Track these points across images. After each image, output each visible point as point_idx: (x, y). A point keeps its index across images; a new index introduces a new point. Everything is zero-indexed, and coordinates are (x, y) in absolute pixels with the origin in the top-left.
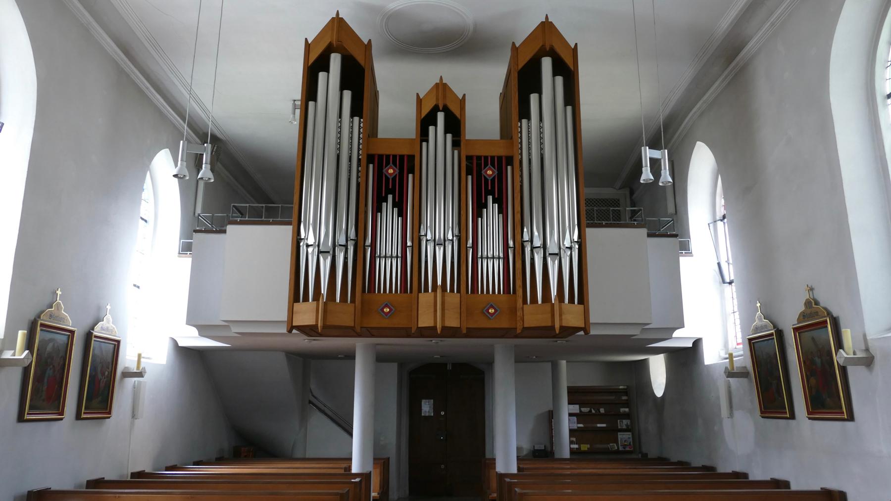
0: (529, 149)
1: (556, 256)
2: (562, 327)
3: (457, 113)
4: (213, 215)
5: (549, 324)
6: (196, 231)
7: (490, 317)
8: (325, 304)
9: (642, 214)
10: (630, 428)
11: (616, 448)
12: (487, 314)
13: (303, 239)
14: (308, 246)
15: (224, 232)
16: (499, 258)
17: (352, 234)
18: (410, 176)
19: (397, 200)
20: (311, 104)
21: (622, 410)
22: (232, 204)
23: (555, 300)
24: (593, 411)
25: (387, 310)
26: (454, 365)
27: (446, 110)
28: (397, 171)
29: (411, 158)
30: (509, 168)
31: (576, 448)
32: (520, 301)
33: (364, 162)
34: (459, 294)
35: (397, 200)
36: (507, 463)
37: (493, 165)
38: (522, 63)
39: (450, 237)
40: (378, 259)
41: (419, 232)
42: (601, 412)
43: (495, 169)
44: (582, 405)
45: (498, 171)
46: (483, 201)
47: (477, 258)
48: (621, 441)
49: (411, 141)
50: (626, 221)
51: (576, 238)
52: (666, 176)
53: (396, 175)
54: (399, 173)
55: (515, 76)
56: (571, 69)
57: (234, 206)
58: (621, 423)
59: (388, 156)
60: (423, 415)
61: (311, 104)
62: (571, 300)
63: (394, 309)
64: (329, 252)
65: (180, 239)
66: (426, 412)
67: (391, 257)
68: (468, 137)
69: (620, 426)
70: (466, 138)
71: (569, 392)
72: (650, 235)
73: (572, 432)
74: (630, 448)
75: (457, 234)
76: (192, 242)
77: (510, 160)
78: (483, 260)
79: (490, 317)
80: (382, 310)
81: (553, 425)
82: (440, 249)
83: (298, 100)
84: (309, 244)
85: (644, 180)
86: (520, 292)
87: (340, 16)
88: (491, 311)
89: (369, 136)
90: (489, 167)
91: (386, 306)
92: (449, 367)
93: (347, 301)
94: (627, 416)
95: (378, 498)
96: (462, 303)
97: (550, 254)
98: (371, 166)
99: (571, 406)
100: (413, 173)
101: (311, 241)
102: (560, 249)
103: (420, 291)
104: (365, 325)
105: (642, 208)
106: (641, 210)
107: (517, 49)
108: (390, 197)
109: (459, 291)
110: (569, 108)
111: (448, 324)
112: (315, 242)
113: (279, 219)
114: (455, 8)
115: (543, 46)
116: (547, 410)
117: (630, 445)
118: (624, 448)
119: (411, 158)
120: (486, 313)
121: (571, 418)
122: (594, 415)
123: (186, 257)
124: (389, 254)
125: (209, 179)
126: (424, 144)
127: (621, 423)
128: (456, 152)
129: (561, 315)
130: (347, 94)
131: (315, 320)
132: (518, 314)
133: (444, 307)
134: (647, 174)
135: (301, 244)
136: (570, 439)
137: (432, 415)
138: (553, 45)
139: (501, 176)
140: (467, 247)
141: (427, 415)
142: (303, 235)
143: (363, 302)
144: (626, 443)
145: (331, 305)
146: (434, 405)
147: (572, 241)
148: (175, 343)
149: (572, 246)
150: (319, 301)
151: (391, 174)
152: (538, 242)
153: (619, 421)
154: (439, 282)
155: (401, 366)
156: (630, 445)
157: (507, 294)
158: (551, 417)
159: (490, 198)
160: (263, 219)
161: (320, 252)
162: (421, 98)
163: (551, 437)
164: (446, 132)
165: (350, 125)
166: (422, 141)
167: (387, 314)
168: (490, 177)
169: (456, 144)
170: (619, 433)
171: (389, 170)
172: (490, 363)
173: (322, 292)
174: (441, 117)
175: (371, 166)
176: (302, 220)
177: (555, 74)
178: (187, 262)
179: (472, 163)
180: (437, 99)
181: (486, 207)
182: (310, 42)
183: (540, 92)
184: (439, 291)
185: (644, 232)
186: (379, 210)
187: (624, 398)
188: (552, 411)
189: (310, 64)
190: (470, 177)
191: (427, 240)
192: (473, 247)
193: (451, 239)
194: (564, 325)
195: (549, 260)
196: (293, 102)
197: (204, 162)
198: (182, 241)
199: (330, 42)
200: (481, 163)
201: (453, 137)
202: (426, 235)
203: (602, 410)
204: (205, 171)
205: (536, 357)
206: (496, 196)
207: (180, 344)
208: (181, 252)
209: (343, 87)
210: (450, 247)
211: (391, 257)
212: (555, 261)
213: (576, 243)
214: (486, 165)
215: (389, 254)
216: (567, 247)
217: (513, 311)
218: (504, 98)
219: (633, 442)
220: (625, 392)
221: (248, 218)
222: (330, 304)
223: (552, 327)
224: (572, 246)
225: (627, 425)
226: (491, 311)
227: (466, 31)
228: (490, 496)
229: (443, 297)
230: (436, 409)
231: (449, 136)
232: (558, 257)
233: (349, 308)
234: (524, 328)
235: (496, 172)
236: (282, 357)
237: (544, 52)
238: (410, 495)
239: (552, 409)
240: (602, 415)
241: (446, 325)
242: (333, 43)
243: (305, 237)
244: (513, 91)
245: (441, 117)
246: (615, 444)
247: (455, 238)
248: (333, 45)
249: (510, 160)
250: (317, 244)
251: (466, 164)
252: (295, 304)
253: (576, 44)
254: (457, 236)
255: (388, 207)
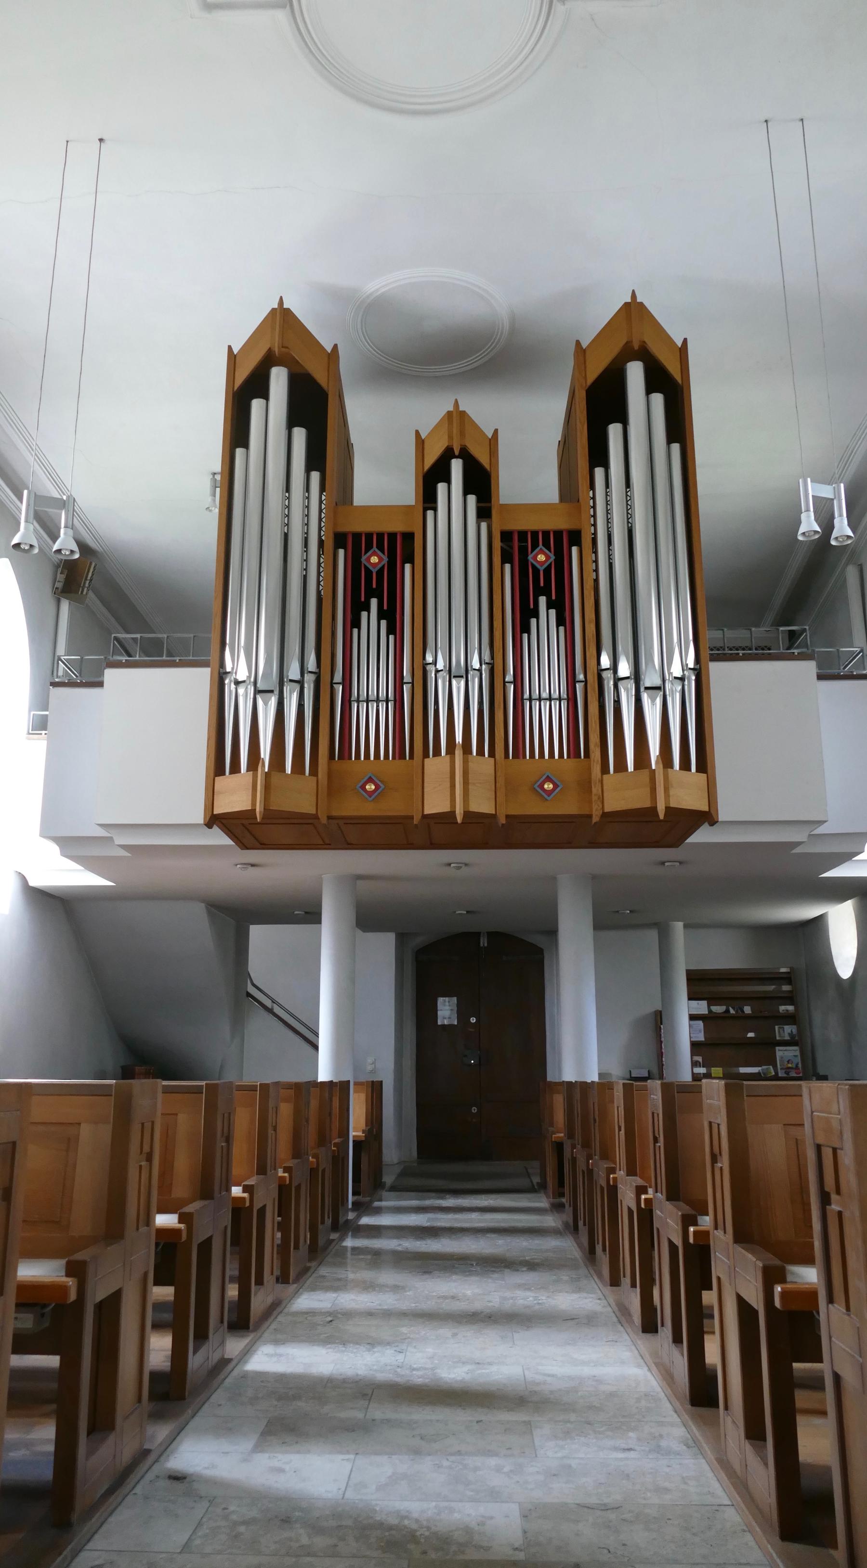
0: (608, 521)
1: (657, 691)
2: (668, 809)
3: (484, 460)
4: (82, 658)
5: (647, 804)
6: (54, 684)
7: (546, 796)
8: (267, 775)
9: (806, 638)
10: (797, 1038)
11: (774, 1074)
12: (541, 792)
13: (229, 673)
14: (237, 683)
15: (100, 684)
16: (560, 699)
17: (311, 664)
18: (408, 567)
19: (385, 607)
20: (239, 452)
21: (782, 1008)
22: (113, 635)
23: (657, 762)
24: (732, 1011)
25: (370, 787)
26: (491, 935)
27: (466, 455)
28: (385, 559)
29: (409, 537)
30: (575, 550)
31: (703, 1074)
32: (596, 769)
33: (329, 545)
34: (493, 759)
35: (385, 607)
36: (581, 1062)
37: (547, 545)
38: (593, 374)
39: (476, 664)
40: (356, 705)
41: (424, 658)
42: (746, 1012)
43: (550, 551)
44: (712, 1000)
45: (555, 555)
46: (532, 606)
47: (523, 699)
48: (781, 1061)
49: (407, 510)
50: (780, 650)
51: (691, 664)
52: (841, 528)
53: (383, 566)
54: (388, 562)
55: (581, 395)
56: (678, 383)
57: (116, 639)
58: (781, 1031)
59: (369, 536)
60: (439, 1023)
61: (239, 452)
62: (685, 764)
63: (382, 786)
64: (272, 691)
65: (30, 711)
66: (444, 1018)
67: (378, 700)
68: (502, 501)
69: (780, 1036)
70: (501, 502)
71: (688, 980)
72: (820, 677)
73: (695, 1046)
74: (798, 1074)
75: (487, 661)
76: (47, 716)
77: (575, 537)
78: (533, 702)
79: (546, 796)
80: (363, 787)
81: (662, 1035)
82: (459, 683)
83: (218, 473)
84: (240, 680)
85: (804, 534)
86: (596, 753)
87: (285, 306)
88: (548, 786)
89: (336, 504)
90: (541, 549)
91: (370, 780)
92: (484, 942)
93: (303, 773)
94: (790, 1019)
95: (363, 1139)
96: (498, 774)
97: (647, 688)
98: (341, 552)
99: (694, 1003)
100: (411, 561)
101: (242, 674)
102: (664, 681)
103: (426, 755)
104: (335, 813)
105: (807, 628)
106: (805, 630)
107: (584, 351)
108: (374, 602)
109: (492, 754)
110: (676, 447)
111: (474, 807)
112: (249, 677)
113: (191, 658)
114: (480, 288)
115: (627, 343)
116: (654, 1010)
117: (797, 1067)
118: (787, 1073)
119: (409, 537)
120: (539, 790)
121: (693, 1022)
122: (733, 1017)
123: (38, 739)
124: (373, 694)
125: (72, 552)
126: (430, 513)
127: (781, 1031)
128: (484, 526)
129: (667, 789)
130: (300, 435)
131: (250, 802)
132: (594, 790)
133: (468, 779)
134: (809, 523)
135: (227, 682)
136: (692, 1058)
137: (456, 1023)
138: (646, 340)
139: (561, 564)
140: (504, 682)
141: (446, 1022)
142: (229, 667)
143: (330, 775)
144: (790, 1065)
145: (276, 778)
146: (459, 1005)
147: (684, 667)
148: (24, 880)
149: (684, 675)
150: (257, 770)
151: (374, 565)
152: (624, 670)
153: (777, 1027)
154: (459, 738)
155: (402, 939)
156: (797, 1067)
157: (575, 757)
158: (659, 1022)
159: (543, 600)
160: (164, 658)
161: (257, 692)
162: (423, 438)
163: (660, 1055)
164: (466, 491)
165: (303, 511)
166: (425, 510)
167: (370, 793)
168: (541, 566)
169: (484, 513)
170: (777, 1048)
171: (372, 558)
172: (552, 933)
173: (262, 756)
174: (457, 467)
175: (341, 552)
176: (228, 641)
177: (650, 389)
178: (40, 745)
179: (512, 547)
180: (450, 437)
181: (537, 616)
182: (236, 351)
183: (624, 420)
184: (459, 753)
185: (810, 667)
186: (356, 623)
187: (786, 988)
188: (661, 1012)
189: (236, 388)
190: (508, 567)
191: (437, 671)
192: (515, 682)
193: (477, 668)
194: (672, 805)
195: (645, 697)
196: (211, 476)
197: (63, 525)
198: (32, 713)
199: (270, 348)
200: (527, 546)
201: (479, 501)
202: (435, 663)
203: (747, 1010)
204: (64, 540)
205: (630, 911)
206: (554, 598)
207: (33, 883)
208: (31, 732)
209: (293, 421)
210: (477, 680)
211: (378, 700)
212: (655, 699)
213: (691, 671)
214: (535, 546)
215: (373, 694)
216: (676, 678)
217: (585, 785)
218: (566, 446)
219: (803, 1060)
220: (788, 978)
221: (139, 657)
222: (276, 778)
223: (653, 810)
224: (684, 675)
225: (791, 1034)
226: (548, 786)
227: (498, 329)
228: (554, 1136)
229: (465, 762)
230: (462, 1014)
231: (472, 499)
232: (662, 693)
233: (307, 782)
234: (605, 815)
235: (553, 558)
236: (200, 910)
237: (629, 353)
238: (418, 1157)
239: (660, 1009)
240: (748, 1017)
241: (471, 810)
242: (275, 351)
243: (233, 668)
244: (578, 423)
245: (457, 467)
246: (771, 1067)
247: (484, 666)
248: (275, 354)
249: (575, 537)
250: (252, 679)
251: (501, 547)
252: (216, 778)
253: (685, 341)
254: (487, 663)
255: (370, 619)
